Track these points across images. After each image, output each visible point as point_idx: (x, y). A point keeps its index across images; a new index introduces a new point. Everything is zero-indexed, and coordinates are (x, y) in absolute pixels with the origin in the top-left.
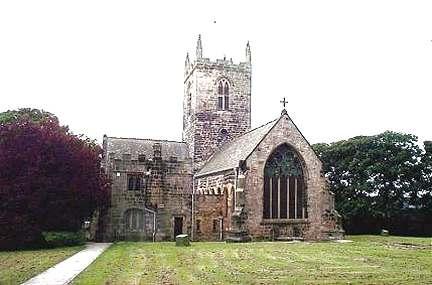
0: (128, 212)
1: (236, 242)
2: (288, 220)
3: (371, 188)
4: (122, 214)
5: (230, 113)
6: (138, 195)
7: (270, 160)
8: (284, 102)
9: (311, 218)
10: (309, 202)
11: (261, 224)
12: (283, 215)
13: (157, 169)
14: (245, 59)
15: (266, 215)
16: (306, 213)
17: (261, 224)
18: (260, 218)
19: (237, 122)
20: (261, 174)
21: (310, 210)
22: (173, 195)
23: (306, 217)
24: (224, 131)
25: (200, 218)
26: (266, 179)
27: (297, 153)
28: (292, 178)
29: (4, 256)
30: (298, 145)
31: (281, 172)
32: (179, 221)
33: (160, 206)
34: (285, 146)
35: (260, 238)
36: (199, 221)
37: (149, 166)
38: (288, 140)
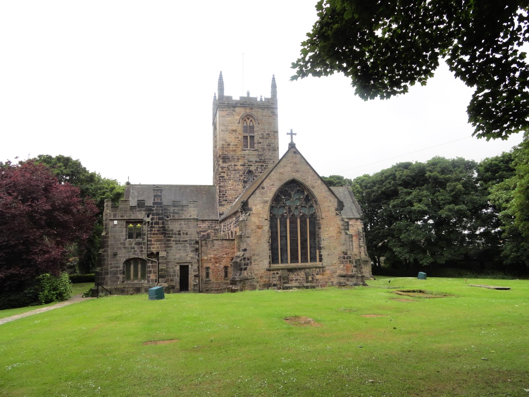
0: (128, 262)
1: (403, 295)
2: (300, 264)
3: (465, 228)
4: (121, 265)
5: (256, 153)
6: (138, 244)
7: (277, 199)
8: (292, 134)
9: (326, 261)
10: (323, 244)
11: (269, 270)
12: (294, 259)
13: (158, 214)
14: (269, 96)
15: (274, 259)
16: (321, 256)
17: (269, 270)
18: (265, 263)
19: (264, 162)
20: (266, 214)
21: (324, 253)
22: (177, 242)
23: (321, 260)
24: (250, 172)
25: (210, 265)
26: (273, 219)
27: (308, 190)
28: (303, 222)
29: (1, 311)
30: (309, 181)
31: (290, 211)
32: (184, 270)
33: (162, 254)
34: (293, 183)
35: (268, 286)
36: (208, 268)
37: (149, 211)
38: (298, 176)
